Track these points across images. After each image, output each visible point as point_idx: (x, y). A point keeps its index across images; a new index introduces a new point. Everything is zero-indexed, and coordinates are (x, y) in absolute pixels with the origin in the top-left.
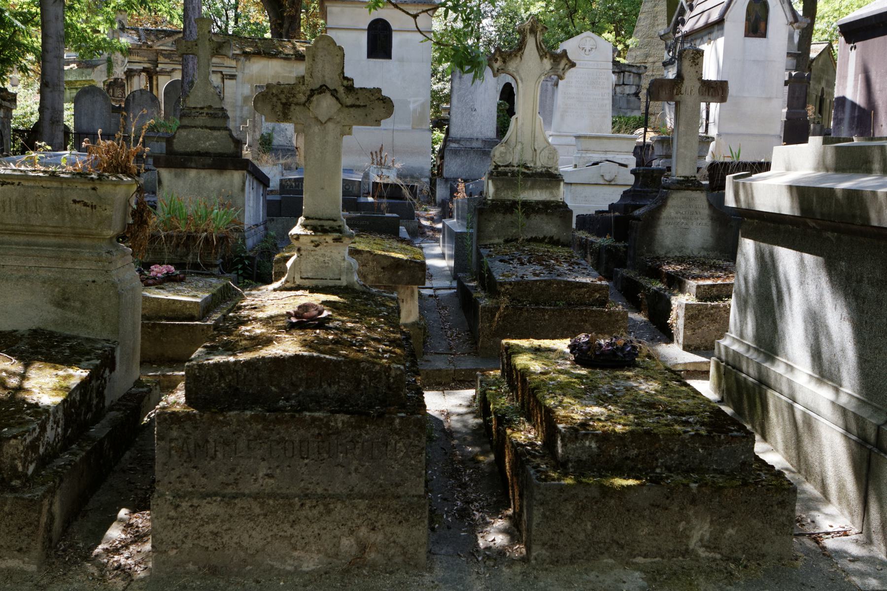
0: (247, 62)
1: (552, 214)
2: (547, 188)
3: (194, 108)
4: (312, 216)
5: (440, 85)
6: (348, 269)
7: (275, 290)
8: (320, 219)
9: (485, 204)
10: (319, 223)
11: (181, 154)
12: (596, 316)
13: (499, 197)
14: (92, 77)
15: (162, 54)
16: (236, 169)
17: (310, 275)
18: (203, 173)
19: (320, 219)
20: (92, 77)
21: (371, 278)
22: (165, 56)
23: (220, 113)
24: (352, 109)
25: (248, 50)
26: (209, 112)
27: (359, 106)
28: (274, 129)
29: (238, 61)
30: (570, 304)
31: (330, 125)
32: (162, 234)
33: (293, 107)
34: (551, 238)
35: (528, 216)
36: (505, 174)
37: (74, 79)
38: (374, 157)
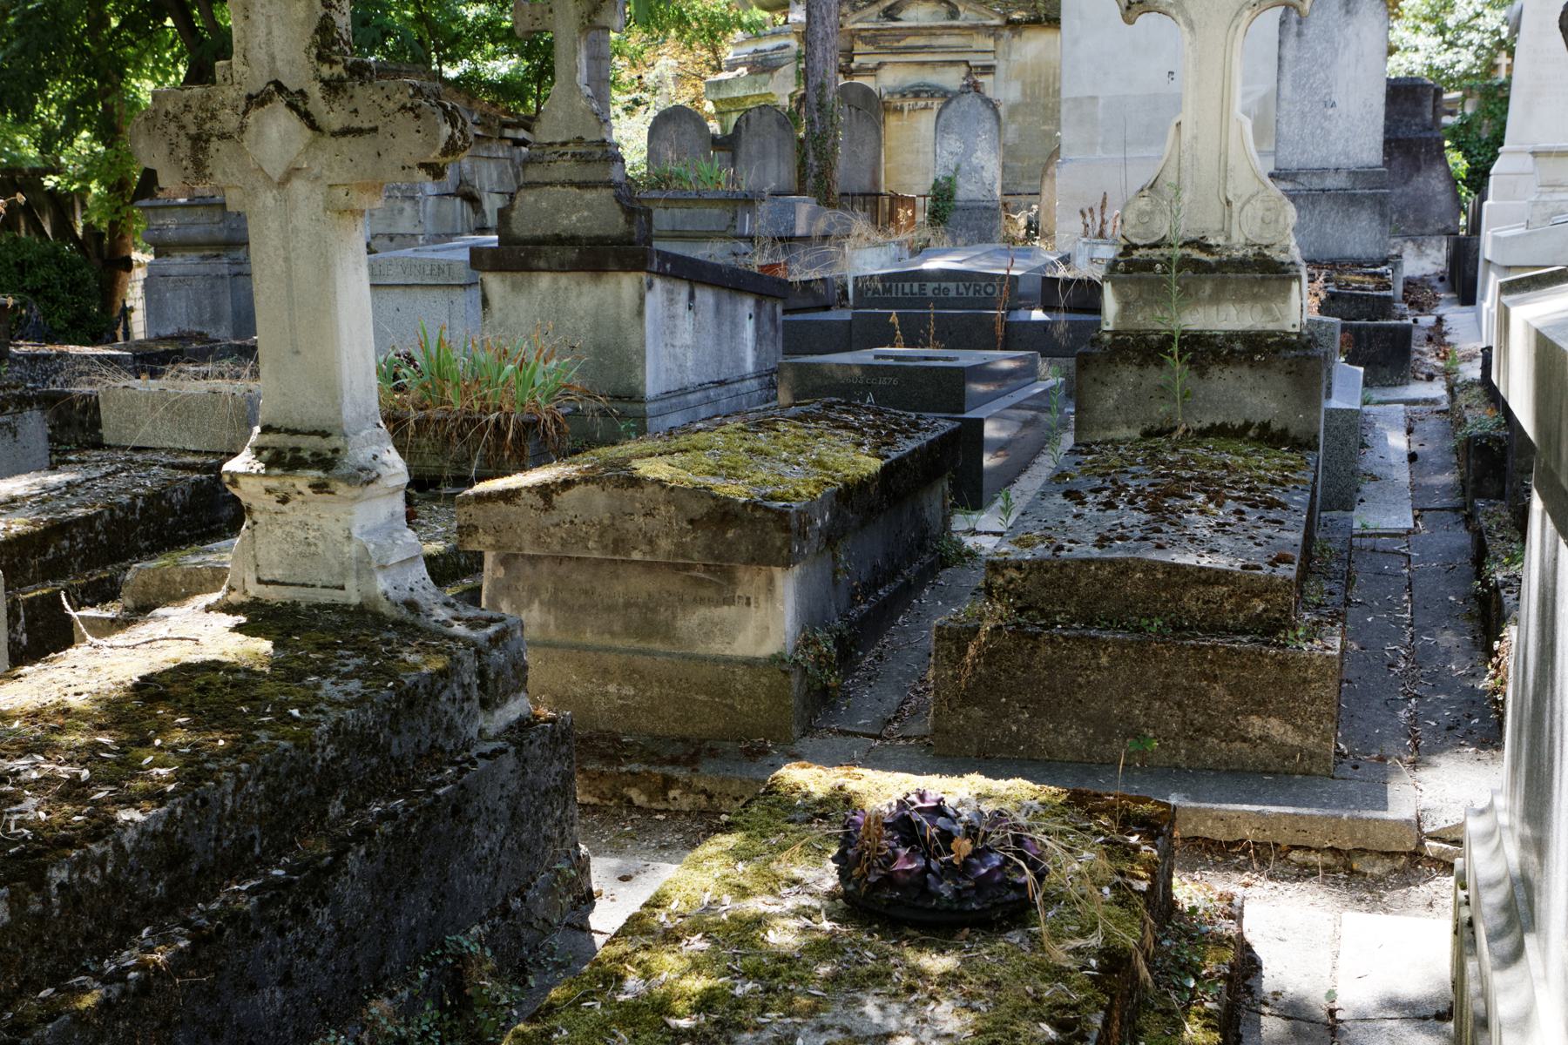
0: (1016, 39)
1: (1266, 365)
2: (1255, 298)
3: (551, 144)
4: (277, 423)
5: (1449, 56)
6: (359, 561)
7: (208, 609)
8: (295, 432)
9: (1096, 342)
10: (292, 441)
11: (526, 242)
12: (1243, 667)
13: (1129, 326)
14: (770, 88)
15: (861, 38)
16: (626, 268)
17: (278, 574)
18: (564, 279)
19: (295, 432)
20: (770, 88)
21: (665, 544)
22: (866, 41)
23: (599, 152)
24: (343, 140)
25: (1016, 16)
26: (578, 150)
27: (359, 132)
28: (958, 168)
29: (997, 38)
30: (1178, 628)
31: (299, 186)
32: (414, 415)
33: (215, 144)
34: (1265, 426)
35: (1202, 373)
36: (1148, 265)
37: (741, 94)
38: (1089, 220)
